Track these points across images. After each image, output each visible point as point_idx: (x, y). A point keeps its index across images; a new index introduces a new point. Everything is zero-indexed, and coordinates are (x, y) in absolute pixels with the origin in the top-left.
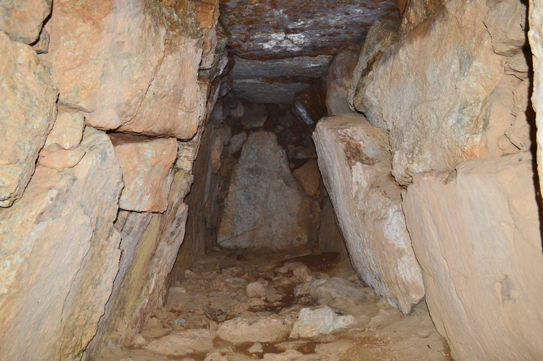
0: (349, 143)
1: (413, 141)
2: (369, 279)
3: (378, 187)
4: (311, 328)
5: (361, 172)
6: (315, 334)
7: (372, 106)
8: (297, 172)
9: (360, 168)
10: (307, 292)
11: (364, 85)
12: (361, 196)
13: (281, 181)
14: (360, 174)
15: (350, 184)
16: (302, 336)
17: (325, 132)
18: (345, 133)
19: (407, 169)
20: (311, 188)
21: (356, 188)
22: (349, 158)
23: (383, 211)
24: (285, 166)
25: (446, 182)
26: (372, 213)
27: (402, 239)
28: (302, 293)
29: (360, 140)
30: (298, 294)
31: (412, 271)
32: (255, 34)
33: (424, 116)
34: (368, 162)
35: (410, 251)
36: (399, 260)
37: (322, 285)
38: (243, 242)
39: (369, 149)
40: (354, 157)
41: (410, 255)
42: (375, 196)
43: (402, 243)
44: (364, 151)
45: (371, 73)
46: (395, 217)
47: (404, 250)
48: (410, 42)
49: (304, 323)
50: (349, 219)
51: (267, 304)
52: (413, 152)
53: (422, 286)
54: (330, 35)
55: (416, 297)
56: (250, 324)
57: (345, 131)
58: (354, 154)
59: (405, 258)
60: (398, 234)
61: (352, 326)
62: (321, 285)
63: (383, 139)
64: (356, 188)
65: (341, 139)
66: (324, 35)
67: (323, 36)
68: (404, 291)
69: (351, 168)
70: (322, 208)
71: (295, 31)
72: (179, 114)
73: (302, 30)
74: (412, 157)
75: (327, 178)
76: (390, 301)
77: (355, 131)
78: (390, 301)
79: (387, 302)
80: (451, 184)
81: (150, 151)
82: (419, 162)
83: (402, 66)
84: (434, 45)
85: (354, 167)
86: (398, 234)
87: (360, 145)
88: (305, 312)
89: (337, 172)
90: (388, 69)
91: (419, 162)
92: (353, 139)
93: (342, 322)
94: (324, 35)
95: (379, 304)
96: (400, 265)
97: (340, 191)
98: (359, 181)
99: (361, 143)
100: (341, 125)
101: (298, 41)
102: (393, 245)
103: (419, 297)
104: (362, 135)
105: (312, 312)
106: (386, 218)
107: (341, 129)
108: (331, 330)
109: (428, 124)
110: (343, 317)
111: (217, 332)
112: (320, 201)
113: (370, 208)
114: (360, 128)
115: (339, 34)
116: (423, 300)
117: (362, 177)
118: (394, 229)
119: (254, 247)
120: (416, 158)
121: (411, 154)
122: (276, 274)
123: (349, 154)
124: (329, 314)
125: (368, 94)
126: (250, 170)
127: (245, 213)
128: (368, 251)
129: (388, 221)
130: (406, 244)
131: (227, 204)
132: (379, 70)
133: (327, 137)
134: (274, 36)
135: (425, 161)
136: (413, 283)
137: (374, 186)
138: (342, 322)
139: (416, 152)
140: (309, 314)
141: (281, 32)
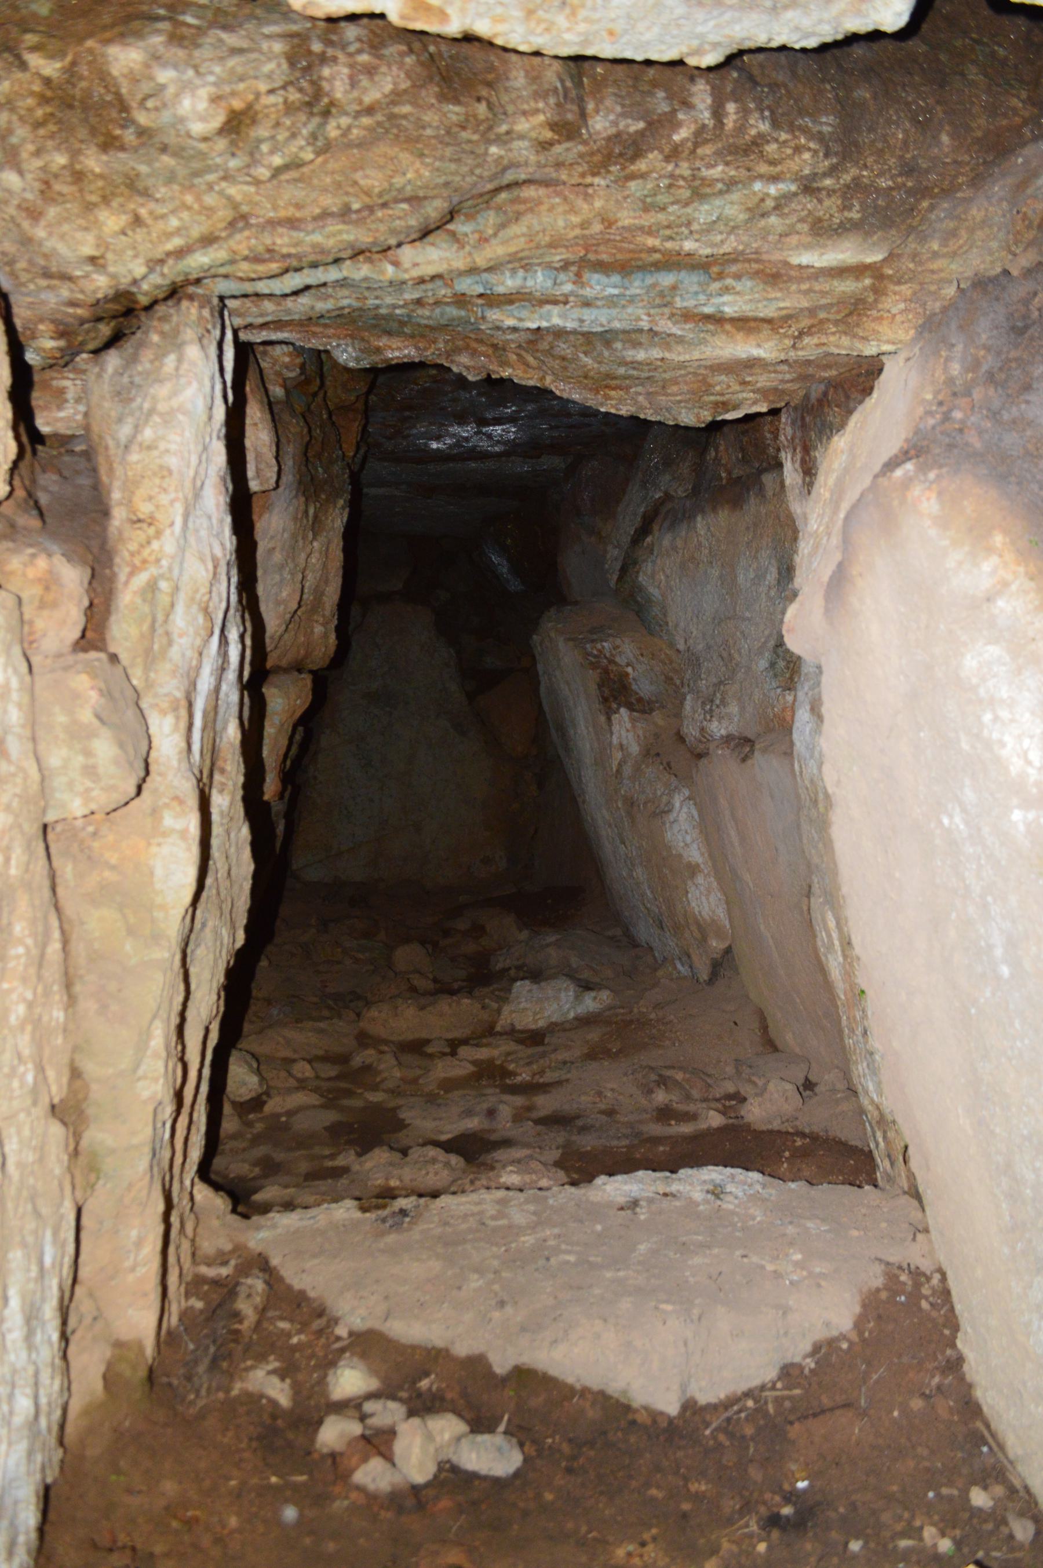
0: (606, 671)
1: (715, 680)
2: (644, 931)
3: (658, 754)
4: (535, 1014)
5: (629, 725)
6: (541, 1023)
7: (649, 600)
9: (626, 719)
10: (520, 963)
11: (635, 563)
12: (627, 770)
14: (625, 731)
15: (607, 744)
16: (518, 1027)
17: (561, 644)
18: (600, 651)
19: (702, 729)
22: (605, 700)
23: (665, 799)
25: (744, 760)
26: (645, 803)
27: (695, 846)
28: (508, 963)
29: (628, 665)
30: (500, 966)
31: (711, 900)
32: (414, 426)
33: (731, 641)
34: (641, 707)
36: (689, 882)
37: (551, 948)
39: (644, 687)
40: (615, 698)
41: (708, 874)
42: (650, 771)
44: (634, 687)
45: (649, 539)
46: (685, 809)
47: (698, 865)
48: (714, 509)
49: (522, 1006)
50: (604, 812)
51: (438, 986)
52: (712, 701)
53: (727, 923)
54: (572, 426)
55: (716, 945)
56: (422, 1008)
57: (599, 646)
58: (615, 691)
59: (700, 879)
60: (688, 839)
61: (610, 1008)
62: (548, 945)
63: (671, 662)
64: (618, 755)
65: (591, 663)
66: (557, 427)
67: (551, 428)
68: (699, 936)
69: (609, 719)
71: (497, 421)
72: (316, 630)
73: (512, 420)
74: (711, 710)
75: (562, 729)
76: (679, 966)
77: (618, 647)
78: (679, 966)
79: (675, 968)
80: (749, 762)
81: (280, 701)
82: (720, 719)
83: (700, 544)
84: (748, 528)
85: (615, 717)
86: (688, 839)
87: (627, 674)
88: (522, 988)
89: (582, 723)
91: (720, 719)
92: (615, 663)
93: (590, 1003)
94: (557, 427)
95: (660, 973)
96: (692, 889)
97: (588, 759)
98: (625, 742)
99: (629, 670)
100: (592, 631)
101: (501, 436)
102: (680, 856)
103: (723, 946)
104: (631, 655)
105: (535, 987)
106: (670, 811)
107: (593, 641)
108: (572, 1015)
109: (736, 656)
110: (593, 994)
111: (361, 1024)
113: (644, 792)
114: (627, 640)
115: (589, 425)
116: (728, 951)
117: (630, 735)
118: (682, 831)
120: (717, 711)
121: (710, 704)
122: (446, 933)
123: (607, 692)
124: (567, 989)
125: (642, 578)
128: (639, 873)
129: (672, 816)
130: (702, 854)
131: (315, 778)
132: (663, 539)
133: (564, 663)
134: (455, 429)
135: (730, 717)
136: (713, 920)
137: (650, 753)
138: (590, 1003)
139: (718, 702)
140: (530, 991)
141: (468, 424)
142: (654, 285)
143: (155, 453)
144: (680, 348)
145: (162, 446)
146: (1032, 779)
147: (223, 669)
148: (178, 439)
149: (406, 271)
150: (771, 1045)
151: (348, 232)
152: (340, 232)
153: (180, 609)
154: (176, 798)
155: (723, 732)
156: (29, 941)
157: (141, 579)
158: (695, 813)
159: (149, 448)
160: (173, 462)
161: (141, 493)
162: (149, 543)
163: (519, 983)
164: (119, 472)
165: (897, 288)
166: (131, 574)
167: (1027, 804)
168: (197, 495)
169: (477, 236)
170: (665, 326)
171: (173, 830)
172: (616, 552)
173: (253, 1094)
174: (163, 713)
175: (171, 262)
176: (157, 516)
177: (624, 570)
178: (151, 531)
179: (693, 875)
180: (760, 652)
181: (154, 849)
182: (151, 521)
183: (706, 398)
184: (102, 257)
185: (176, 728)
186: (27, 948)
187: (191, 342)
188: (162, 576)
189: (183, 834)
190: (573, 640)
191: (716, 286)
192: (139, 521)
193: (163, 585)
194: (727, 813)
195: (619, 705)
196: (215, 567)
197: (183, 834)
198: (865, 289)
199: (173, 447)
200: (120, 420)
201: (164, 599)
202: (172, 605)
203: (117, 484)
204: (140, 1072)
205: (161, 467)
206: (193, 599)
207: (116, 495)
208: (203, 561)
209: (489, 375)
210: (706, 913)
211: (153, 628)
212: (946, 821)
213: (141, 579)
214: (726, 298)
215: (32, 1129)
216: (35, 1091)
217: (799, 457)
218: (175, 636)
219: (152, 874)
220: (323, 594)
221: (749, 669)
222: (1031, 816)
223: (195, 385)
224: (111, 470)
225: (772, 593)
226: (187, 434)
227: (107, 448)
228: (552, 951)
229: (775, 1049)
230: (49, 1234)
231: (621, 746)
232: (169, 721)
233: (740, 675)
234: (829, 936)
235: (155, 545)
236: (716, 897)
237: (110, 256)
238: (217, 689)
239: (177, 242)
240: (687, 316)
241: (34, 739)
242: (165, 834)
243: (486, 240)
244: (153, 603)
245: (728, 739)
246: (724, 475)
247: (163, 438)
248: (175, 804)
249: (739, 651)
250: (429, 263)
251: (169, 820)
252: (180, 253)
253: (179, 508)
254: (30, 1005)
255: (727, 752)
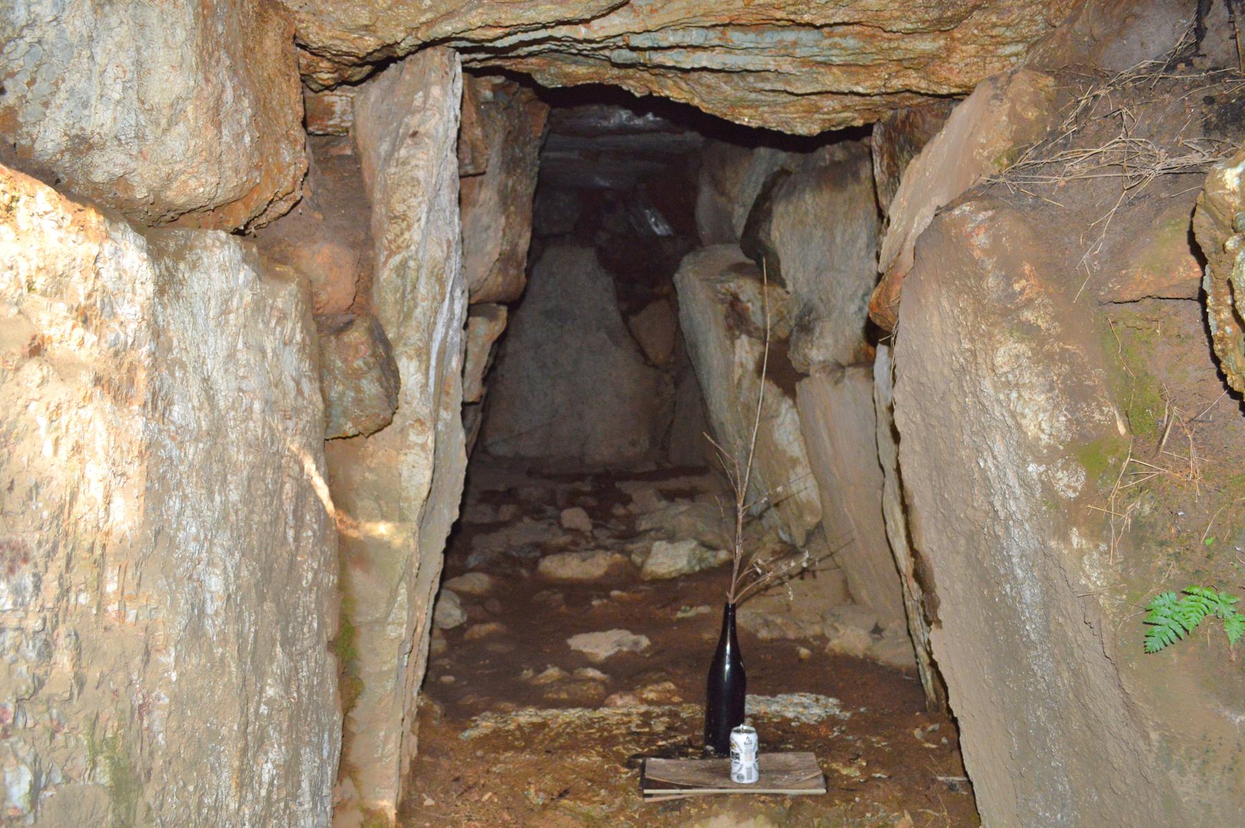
5: (748, 348)
8: (633, 320)
12: (746, 383)
13: (603, 335)
20: (658, 350)
21: (738, 371)
22: (730, 328)
24: (611, 307)
25: (836, 383)
30: (642, 528)
35: (805, 461)
38: (530, 448)
43: (796, 449)
47: (798, 459)
56: (584, 560)
59: (799, 470)
60: (791, 438)
62: (681, 513)
69: (733, 343)
70: (677, 385)
75: (695, 346)
80: (840, 385)
85: (738, 342)
90: (791, 208)
98: (744, 361)
99: (750, 305)
102: (785, 451)
103: (816, 520)
105: (670, 546)
106: (778, 416)
108: (697, 568)
112: (674, 373)
116: (819, 526)
118: (786, 428)
119: (170, 498)
124: (542, 109)
126: (548, 314)
127: (536, 393)
129: (779, 421)
133: (699, 289)
142: (780, 41)
143: (409, 168)
144: (798, 84)
145: (413, 162)
146: (1043, 443)
147: (451, 319)
148: (425, 157)
149: (595, 32)
150: (849, 597)
151: (554, 10)
152: (550, 10)
153: (423, 280)
154: (418, 420)
155: (821, 358)
156: (315, 526)
157: (397, 259)
158: (796, 417)
159: (404, 163)
160: (421, 174)
161: (397, 197)
162: (402, 234)
163: (657, 543)
164: (380, 177)
165: (964, 48)
166: (389, 257)
167: (1039, 460)
168: (437, 192)
169: (649, 8)
170: (786, 67)
171: (416, 444)
172: (742, 210)
173: (457, 624)
174: (410, 358)
175: (424, 28)
176: (410, 214)
177: (748, 227)
178: (404, 225)
179: (793, 467)
180: (851, 299)
181: (402, 458)
182: (404, 217)
183: (816, 116)
184: (374, 25)
185: (419, 370)
186: (314, 533)
187: (435, 84)
188: (410, 257)
189: (423, 446)
190: (707, 280)
191: (827, 42)
192: (396, 217)
193: (412, 264)
194: (821, 422)
195: (741, 332)
196: (449, 247)
197: (423, 446)
198: (940, 48)
199: (422, 163)
200: (381, 139)
201: (411, 274)
202: (418, 279)
203: (378, 187)
204: (390, 619)
205: (412, 178)
206: (432, 272)
207: (378, 196)
208: (440, 245)
209: (651, 93)
210: (803, 495)
211: (403, 296)
212: (982, 464)
213: (397, 259)
214: (834, 52)
215: (316, 662)
216: (319, 634)
217: (885, 162)
218: (419, 300)
219: (400, 475)
220: (517, 245)
221: (843, 310)
222: (1042, 469)
223: (438, 116)
224: (373, 176)
225: (862, 253)
226: (431, 153)
227: (369, 158)
228: (683, 518)
229: (854, 601)
230: (326, 736)
231: (742, 365)
232: (414, 365)
233: (835, 315)
234: (896, 525)
235: (407, 235)
236: (811, 482)
237: (379, 24)
238: (447, 333)
239: (429, 16)
240: (805, 62)
241: (321, 380)
242: (409, 447)
243: (656, 11)
244: (403, 277)
245: (824, 365)
246: (827, 157)
247: (414, 156)
248: (417, 425)
249: (835, 296)
250: (613, 26)
251: (413, 437)
252: (430, 24)
253: (424, 208)
254: (316, 573)
255: (823, 376)
